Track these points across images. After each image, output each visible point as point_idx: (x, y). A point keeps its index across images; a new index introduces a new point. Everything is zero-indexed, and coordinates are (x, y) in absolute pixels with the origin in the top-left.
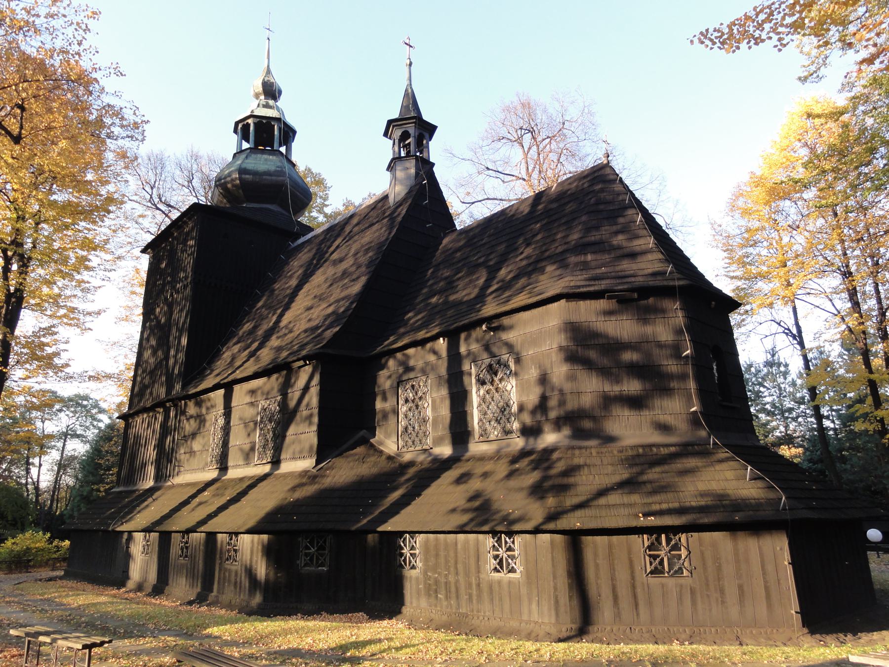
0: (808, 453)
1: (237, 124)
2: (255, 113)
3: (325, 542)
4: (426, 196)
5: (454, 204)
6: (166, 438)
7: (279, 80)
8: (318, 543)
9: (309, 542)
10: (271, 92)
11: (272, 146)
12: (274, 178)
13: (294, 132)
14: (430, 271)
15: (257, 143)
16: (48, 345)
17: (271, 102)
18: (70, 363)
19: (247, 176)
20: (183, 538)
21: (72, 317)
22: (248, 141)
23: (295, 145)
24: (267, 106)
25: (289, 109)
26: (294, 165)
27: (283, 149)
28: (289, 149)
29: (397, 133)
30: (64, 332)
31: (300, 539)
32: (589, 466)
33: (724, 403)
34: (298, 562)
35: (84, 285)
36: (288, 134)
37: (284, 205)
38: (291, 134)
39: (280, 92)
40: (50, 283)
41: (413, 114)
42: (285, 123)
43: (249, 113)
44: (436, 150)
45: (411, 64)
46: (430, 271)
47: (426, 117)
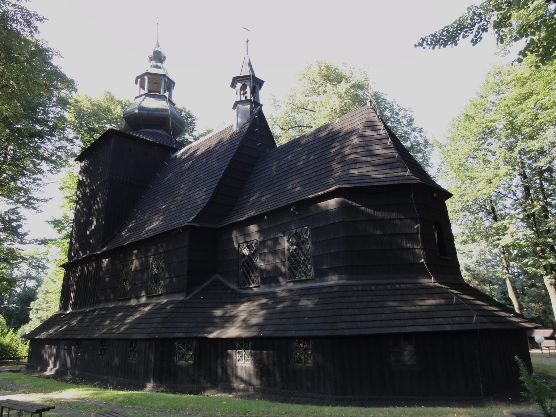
0: (501, 288)
1: (137, 78)
2: (149, 72)
3: (191, 345)
4: (257, 126)
5: (275, 130)
6: (508, 308)
7: (164, 52)
8: (187, 346)
9: (182, 346)
10: (158, 57)
11: (160, 92)
12: (161, 113)
13: (174, 83)
14: (120, 314)
15: (150, 91)
16: (14, 220)
17: (159, 64)
18: (29, 233)
19: (144, 112)
20: (102, 343)
21: (29, 203)
22: (144, 88)
23: (174, 92)
24: (156, 67)
25: (169, 69)
26: (174, 105)
27: (167, 94)
28: (170, 94)
29: (239, 85)
30: (23, 211)
31: (176, 343)
32: (50, 278)
33: (442, 257)
34: (175, 358)
35: (38, 182)
36: (170, 85)
37: (168, 131)
38: (172, 85)
39: (165, 58)
40: (14, 179)
41: (248, 73)
42: (168, 78)
43: (144, 72)
44: (264, 96)
45: (247, 42)
46: (120, 314)
47: (257, 75)
